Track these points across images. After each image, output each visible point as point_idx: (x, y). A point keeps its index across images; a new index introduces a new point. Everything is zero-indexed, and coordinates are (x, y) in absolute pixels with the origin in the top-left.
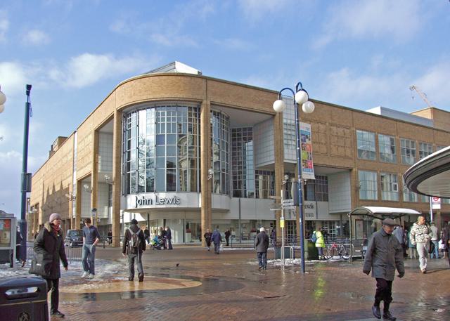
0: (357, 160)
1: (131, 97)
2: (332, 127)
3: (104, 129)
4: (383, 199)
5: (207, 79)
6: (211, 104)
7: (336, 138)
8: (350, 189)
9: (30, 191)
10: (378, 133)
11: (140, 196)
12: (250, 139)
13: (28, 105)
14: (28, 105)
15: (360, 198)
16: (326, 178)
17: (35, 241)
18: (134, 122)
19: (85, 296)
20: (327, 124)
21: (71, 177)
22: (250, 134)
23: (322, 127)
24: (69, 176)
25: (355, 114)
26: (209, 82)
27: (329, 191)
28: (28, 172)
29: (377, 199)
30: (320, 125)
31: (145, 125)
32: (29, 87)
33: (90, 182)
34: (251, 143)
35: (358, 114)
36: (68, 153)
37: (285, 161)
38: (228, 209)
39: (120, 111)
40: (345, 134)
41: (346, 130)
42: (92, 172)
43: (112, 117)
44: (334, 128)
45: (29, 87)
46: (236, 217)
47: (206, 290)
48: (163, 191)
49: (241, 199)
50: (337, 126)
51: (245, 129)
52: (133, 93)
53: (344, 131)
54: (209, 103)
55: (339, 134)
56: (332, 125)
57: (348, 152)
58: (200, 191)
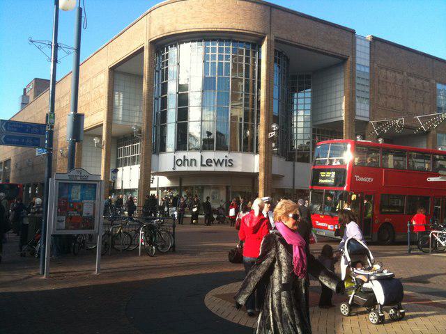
6: (276, 41)
25: (436, 62)
26: (274, 11)
30: (398, 75)
44: (412, 79)
50: (416, 77)
56: (410, 75)
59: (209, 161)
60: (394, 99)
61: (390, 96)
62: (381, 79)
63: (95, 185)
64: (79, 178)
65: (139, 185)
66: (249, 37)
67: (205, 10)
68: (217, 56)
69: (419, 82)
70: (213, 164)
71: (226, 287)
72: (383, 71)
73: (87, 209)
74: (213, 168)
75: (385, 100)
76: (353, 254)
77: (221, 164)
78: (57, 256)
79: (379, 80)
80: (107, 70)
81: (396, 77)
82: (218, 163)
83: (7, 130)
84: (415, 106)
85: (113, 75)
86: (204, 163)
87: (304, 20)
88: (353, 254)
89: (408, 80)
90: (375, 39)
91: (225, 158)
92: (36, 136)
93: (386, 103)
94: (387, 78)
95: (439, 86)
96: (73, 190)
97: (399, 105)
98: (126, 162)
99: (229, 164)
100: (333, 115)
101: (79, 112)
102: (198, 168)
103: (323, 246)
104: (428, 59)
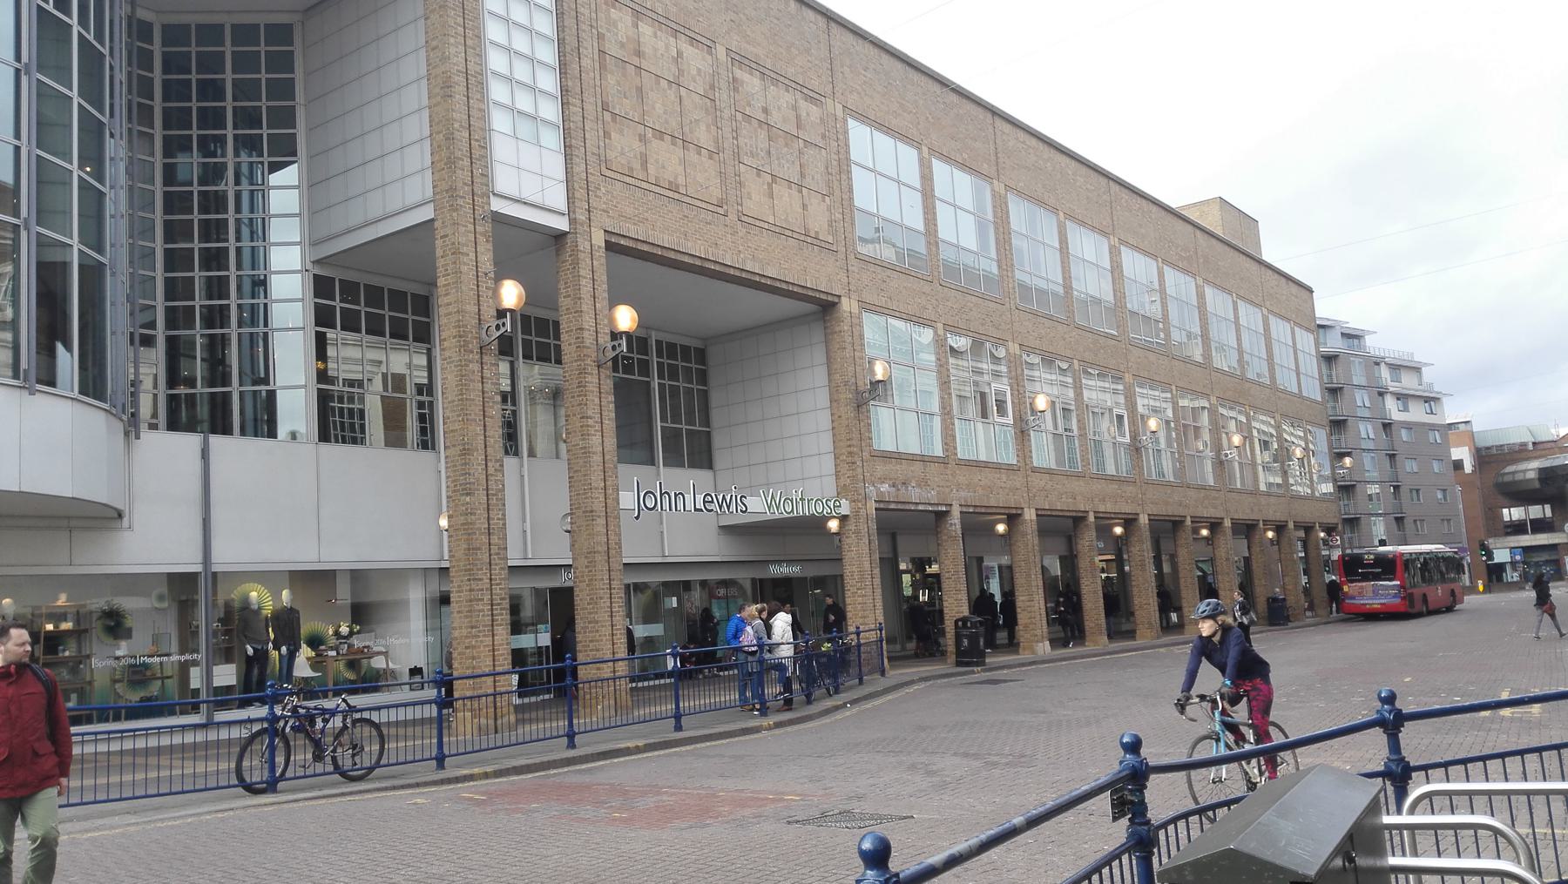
0: (855, 266)
7: (763, 134)
12: (284, 152)
16: (701, 355)
25: (840, 37)
27: (716, 417)
29: (938, 451)
30: (689, 51)
31: (13, 666)
34: (289, 175)
35: (850, 38)
37: (497, 205)
38: (96, 491)
41: (803, 104)
44: (752, 83)
47: (1436, 399)
50: (770, 77)
51: (245, 33)
53: (795, 108)
55: (775, 118)
57: (818, 220)
60: (679, 152)
61: (660, 135)
62: (612, 49)
65: (1387, 824)
68: (193, 391)
69: (782, 99)
73: (1229, 601)
76: (65, 183)
78: (835, 359)
81: (680, 54)
88: (65, 183)
95: (859, 134)
98: (685, 675)
100: (375, 209)
103: (305, 645)
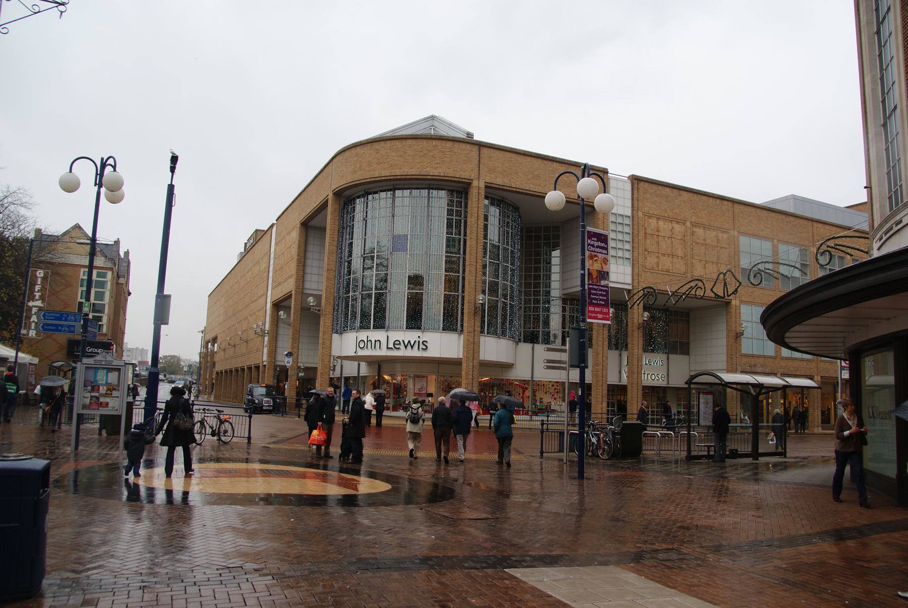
1: (354, 172)
2: (695, 229)
3: (314, 223)
4: (578, 370)
5: (481, 145)
6: (486, 187)
8: (725, 335)
9: (167, 324)
10: (779, 241)
11: (363, 335)
13: (171, 188)
14: (171, 188)
15: (744, 350)
17: (677, 360)
18: (358, 216)
19: (497, 492)
20: (688, 224)
21: (264, 298)
22: (557, 237)
23: (678, 228)
24: (261, 296)
26: (485, 151)
27: (692, 337)
28: (166, 292)
30: (676, 226)
32: (174, 159)
33: (290, 308)
34: (556, 253)
36: (262, 258)
39: (338, 194)
40: (718, 241)
41: (720, 235)
42: (293, 293)
43: (324, 206)
44: (699, 231)
45: (174, 159)
46: (527, 377)
48: (398, 328)
49: (536, 345)
50: (704, 227)
52: (358, 166)
53: (717, 236)
54: (482, 185)
55: (708, 241)
56: (695, 225)
58: (462, 331)
59: (397, 344)
60: (670, 259)
61: (664, 255)
62: (649, 231)
63: (120, 369)
64: (103, 363)
66: (454, 184)
67: (394, 154)
70: (402, 347)
71: (273, 469)
72: (653, 222)
74: (402, 352)
75: (656, 260)
77: (412, 347)
79: (646, 233)
80: (299, 225)
81: (673, 228)
82: (407, 345)
83: (45, 319)
84: (705, 268)
85: (307, 232)
86: (391, 345)
87: (521, 159)
89: (693, 233)
90: (636, 180)
91: (417, 340)
92: (72, 323)
93: (658, 264)
94: (658, 231)
95: (743, 240)
96: (99, 373)
97: (678, 266)
99: (422, 346)
101: (166, 292)
102: (384, 352)
104: (726, 202)
